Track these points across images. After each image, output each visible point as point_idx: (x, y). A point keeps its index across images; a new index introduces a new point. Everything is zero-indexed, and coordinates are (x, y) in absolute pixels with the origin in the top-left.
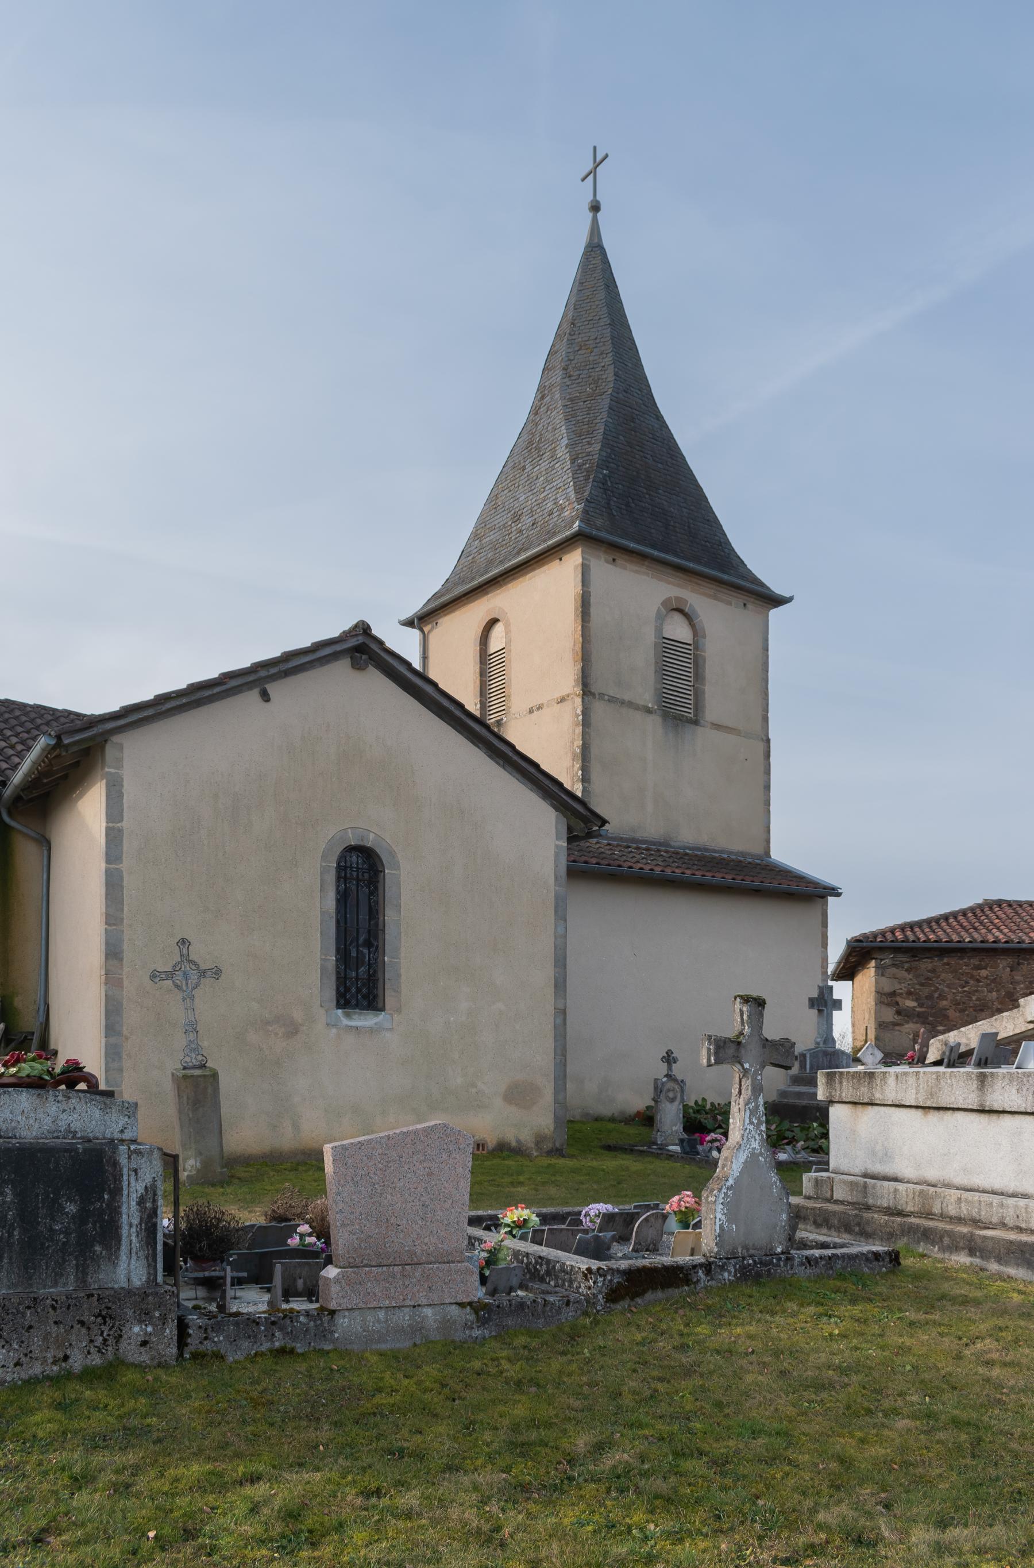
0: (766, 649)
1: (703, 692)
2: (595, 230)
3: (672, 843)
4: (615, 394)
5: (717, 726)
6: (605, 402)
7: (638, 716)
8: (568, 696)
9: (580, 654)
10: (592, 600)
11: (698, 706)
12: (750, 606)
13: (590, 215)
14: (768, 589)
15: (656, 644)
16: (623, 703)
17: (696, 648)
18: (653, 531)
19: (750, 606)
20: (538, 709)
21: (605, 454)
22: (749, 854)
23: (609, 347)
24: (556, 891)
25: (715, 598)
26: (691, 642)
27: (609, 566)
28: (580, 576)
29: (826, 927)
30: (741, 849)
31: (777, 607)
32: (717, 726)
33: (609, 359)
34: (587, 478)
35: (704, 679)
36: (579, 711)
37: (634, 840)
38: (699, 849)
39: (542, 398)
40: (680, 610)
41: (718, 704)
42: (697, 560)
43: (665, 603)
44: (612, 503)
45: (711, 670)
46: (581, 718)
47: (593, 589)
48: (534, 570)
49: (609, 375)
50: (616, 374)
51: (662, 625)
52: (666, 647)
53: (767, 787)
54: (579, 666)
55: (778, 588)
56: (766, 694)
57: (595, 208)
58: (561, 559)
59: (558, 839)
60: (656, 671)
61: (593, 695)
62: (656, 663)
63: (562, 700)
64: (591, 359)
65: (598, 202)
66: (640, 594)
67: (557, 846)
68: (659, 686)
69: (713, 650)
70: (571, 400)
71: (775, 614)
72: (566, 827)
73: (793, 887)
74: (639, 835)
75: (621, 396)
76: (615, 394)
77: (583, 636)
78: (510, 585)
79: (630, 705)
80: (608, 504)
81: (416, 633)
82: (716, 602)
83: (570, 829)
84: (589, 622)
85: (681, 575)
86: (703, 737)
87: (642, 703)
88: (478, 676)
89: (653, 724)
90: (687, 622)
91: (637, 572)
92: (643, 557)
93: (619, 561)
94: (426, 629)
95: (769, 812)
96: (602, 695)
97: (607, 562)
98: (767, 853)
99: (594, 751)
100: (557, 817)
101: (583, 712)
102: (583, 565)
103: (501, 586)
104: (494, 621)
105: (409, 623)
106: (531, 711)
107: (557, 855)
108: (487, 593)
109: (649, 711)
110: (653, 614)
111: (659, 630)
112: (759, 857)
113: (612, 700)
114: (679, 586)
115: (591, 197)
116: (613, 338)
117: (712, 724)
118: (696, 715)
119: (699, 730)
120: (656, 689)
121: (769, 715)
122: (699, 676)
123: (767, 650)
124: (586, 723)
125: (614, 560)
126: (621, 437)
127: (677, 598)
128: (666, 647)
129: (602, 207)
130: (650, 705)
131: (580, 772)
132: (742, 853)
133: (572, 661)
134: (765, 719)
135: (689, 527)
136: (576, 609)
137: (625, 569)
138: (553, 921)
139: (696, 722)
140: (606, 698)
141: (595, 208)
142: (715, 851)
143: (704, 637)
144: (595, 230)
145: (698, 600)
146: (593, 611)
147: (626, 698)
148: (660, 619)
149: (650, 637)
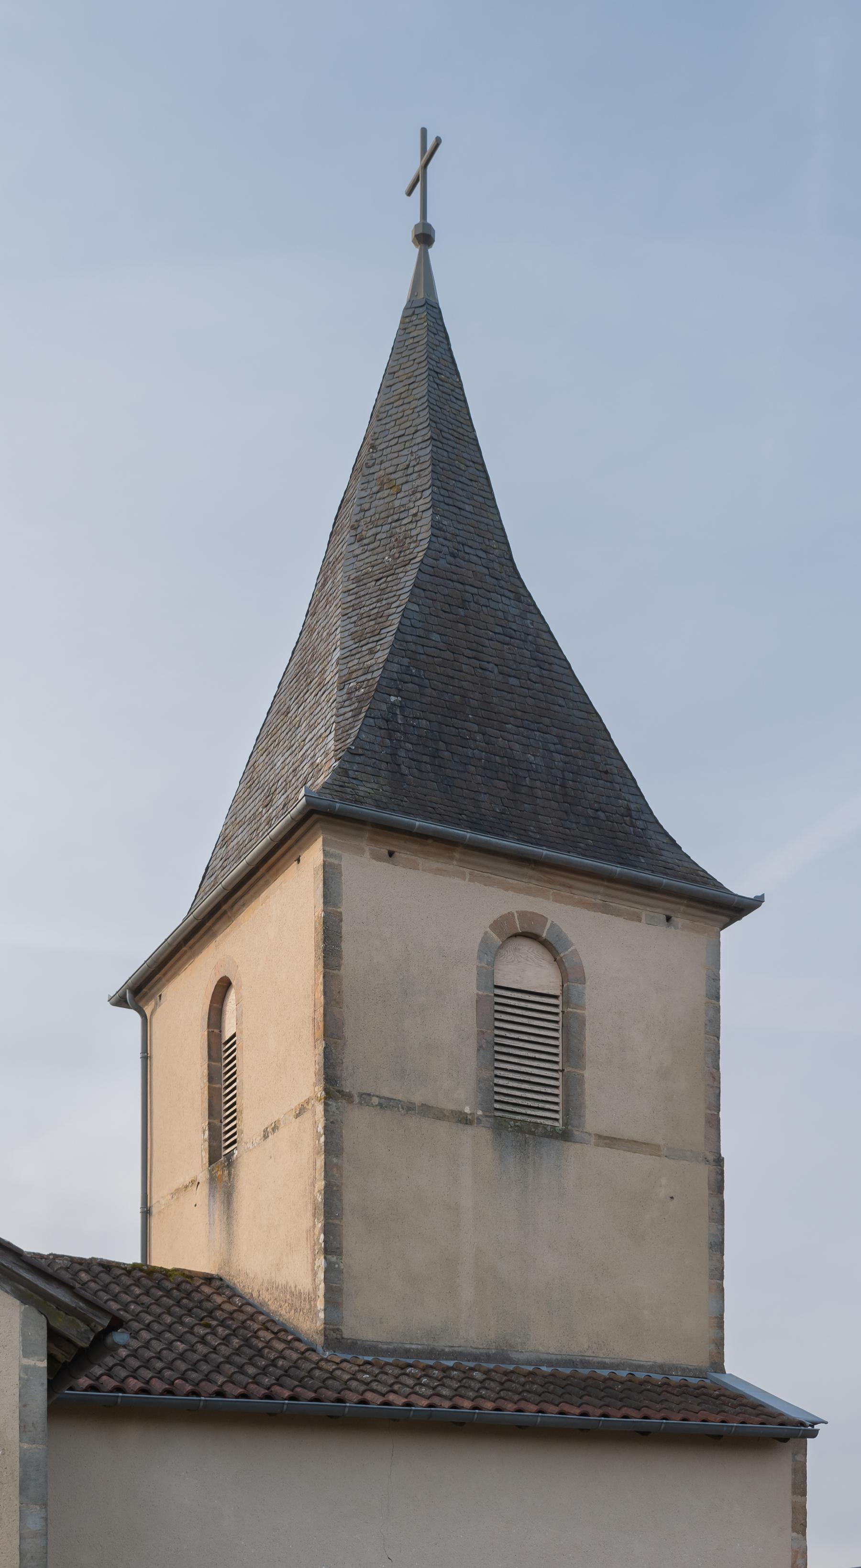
0: (716, 996)
1: (580, 1081)
2: (424, 276)
3: (514, 1355)
4: (431, 561)
5: (609, 1141)
6: (409, 577)
7: (443, 1130)
8: (307, 1102)
9: (321, 1025)
10: (346, 928)
11: (572, 1107)
12: (678, 920)
13: (414, 251)
14: (719, 886)
15: (479, 1000)
16: (410, 1108)
17: (567, 1003)
18: (483, 797)
19: (678, 920)
20: (274, 1130)
21: (396, 667)
22: (676, 1368)
23: (425, 480)
24: (22, 1451)
25: (605, 909)
26: (558, 992)
27: (383, 866)
28: (321, 885)
29: (804, 1493)
30: (659, 1360)
31: (732, 920)
32: (609, 1141)
33: (424, 502)
34: (356, 713)
35: (581, 1056)
36: (321, 1129)
37: (432, 1353)
38: (569, 1363)
39: (324, 585)
40: (531, 934)
41: (606, 1102)
42: (572, 846)
43: (497, 926)
44: (402, 753)
45: (595, 1041)
46: (322, 1139)
47: (345, 908)
48: (267, 884)
49: (423, 530)
50: (435, 526)
51: (492, 964)
52: (502, 1006)
53: (718, 1246)
54: (321, 1045)
55: (740, 886)
56: (715, 1078)
57: (424, 238)
58: (298, 860)
59: (26, 1354)
60: (480, 1048)
61: (349, 1097)
62: (481, 1033)
63: (301, 1111)
64: (397, 503)
65: (429, 227)
66: (442, 915)
67: (25, 1369)
68: (487, 1074)
69: (597, 1004)
70: (358, 580)
71: (733, 937)
72: (44, 1333)
73: (753, 1426)
74: (443, 1343)
75: (442, 563)
76: (431, 561)
77: (325, 993)
78: (241, 918)
79: (426, 1110)
80: (394, 755)
81: (133, 1016)
82: (605, 916)
83: (53, 1335)
84: (338, 967)
85: (531, 872)
86: (579, 1161)
87: (449, 1106)
88: (206, 1080)
89: (476, 1143)
90: (548, 957)
91: (438, 872)
92: (448, 844)
93: (400, 855)
94: (148, 1010)
95: (722, 1290)
96: (365, 1098)
97: (377, 858)
98: (718, 1365)
99: (350, 1198)
100: (24, 1315)
101: (325, 1128)
102: (325, 865)
103: (230, 920)
104: (224, 986)
105: (120, 1001)
106: (266, 1137)
107: (24, 1385)
108: (215, 935)
109: (464, 1120)
110: (473, 943)
111: (486, 974)
112: (701, 1374)
113: (387, 1104)
114: (528, 892)
115: (417, 220)
116: (435, 462)
117: (599, 1136)
118: (565, 1124)
119: (573, 1149)
120: (479, 1081)
121: (722, 1115)
122: (573, 1053)
123: (718, 998)
124: (333, 1144)
125: (391, 854)
126: (435, 637)
127: (524, 915)
128: (502, 1006)
129: (437, 237)
130: (467, 1110)
131: (322, 1237)
132: (661, 1366)
133: (311, 1039)
134: (714, 1123)
135: (563, 786)
136: (317, 946)
137: (415, 867)
138: (16, 1503)
139: (565, 1136)
140: (375, 1101)
141: (424, 238)
142: (603, 1365)
143: (583, 980)
144: (424, 276)
145: (574, 918)
146: (347, 947)
147: (417, 1098)
148: (490, 954)
149: (466, 986)
